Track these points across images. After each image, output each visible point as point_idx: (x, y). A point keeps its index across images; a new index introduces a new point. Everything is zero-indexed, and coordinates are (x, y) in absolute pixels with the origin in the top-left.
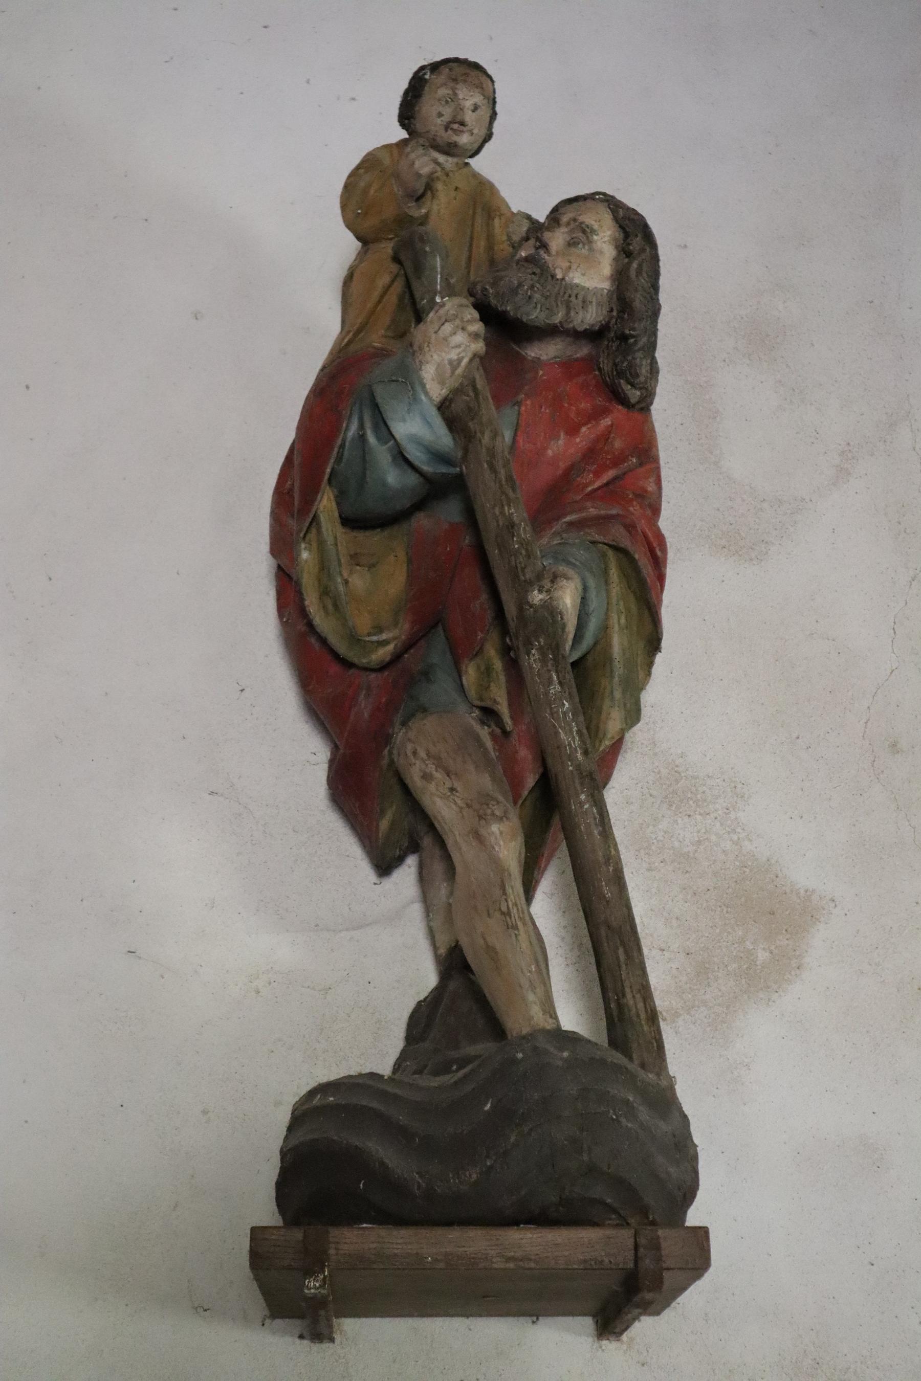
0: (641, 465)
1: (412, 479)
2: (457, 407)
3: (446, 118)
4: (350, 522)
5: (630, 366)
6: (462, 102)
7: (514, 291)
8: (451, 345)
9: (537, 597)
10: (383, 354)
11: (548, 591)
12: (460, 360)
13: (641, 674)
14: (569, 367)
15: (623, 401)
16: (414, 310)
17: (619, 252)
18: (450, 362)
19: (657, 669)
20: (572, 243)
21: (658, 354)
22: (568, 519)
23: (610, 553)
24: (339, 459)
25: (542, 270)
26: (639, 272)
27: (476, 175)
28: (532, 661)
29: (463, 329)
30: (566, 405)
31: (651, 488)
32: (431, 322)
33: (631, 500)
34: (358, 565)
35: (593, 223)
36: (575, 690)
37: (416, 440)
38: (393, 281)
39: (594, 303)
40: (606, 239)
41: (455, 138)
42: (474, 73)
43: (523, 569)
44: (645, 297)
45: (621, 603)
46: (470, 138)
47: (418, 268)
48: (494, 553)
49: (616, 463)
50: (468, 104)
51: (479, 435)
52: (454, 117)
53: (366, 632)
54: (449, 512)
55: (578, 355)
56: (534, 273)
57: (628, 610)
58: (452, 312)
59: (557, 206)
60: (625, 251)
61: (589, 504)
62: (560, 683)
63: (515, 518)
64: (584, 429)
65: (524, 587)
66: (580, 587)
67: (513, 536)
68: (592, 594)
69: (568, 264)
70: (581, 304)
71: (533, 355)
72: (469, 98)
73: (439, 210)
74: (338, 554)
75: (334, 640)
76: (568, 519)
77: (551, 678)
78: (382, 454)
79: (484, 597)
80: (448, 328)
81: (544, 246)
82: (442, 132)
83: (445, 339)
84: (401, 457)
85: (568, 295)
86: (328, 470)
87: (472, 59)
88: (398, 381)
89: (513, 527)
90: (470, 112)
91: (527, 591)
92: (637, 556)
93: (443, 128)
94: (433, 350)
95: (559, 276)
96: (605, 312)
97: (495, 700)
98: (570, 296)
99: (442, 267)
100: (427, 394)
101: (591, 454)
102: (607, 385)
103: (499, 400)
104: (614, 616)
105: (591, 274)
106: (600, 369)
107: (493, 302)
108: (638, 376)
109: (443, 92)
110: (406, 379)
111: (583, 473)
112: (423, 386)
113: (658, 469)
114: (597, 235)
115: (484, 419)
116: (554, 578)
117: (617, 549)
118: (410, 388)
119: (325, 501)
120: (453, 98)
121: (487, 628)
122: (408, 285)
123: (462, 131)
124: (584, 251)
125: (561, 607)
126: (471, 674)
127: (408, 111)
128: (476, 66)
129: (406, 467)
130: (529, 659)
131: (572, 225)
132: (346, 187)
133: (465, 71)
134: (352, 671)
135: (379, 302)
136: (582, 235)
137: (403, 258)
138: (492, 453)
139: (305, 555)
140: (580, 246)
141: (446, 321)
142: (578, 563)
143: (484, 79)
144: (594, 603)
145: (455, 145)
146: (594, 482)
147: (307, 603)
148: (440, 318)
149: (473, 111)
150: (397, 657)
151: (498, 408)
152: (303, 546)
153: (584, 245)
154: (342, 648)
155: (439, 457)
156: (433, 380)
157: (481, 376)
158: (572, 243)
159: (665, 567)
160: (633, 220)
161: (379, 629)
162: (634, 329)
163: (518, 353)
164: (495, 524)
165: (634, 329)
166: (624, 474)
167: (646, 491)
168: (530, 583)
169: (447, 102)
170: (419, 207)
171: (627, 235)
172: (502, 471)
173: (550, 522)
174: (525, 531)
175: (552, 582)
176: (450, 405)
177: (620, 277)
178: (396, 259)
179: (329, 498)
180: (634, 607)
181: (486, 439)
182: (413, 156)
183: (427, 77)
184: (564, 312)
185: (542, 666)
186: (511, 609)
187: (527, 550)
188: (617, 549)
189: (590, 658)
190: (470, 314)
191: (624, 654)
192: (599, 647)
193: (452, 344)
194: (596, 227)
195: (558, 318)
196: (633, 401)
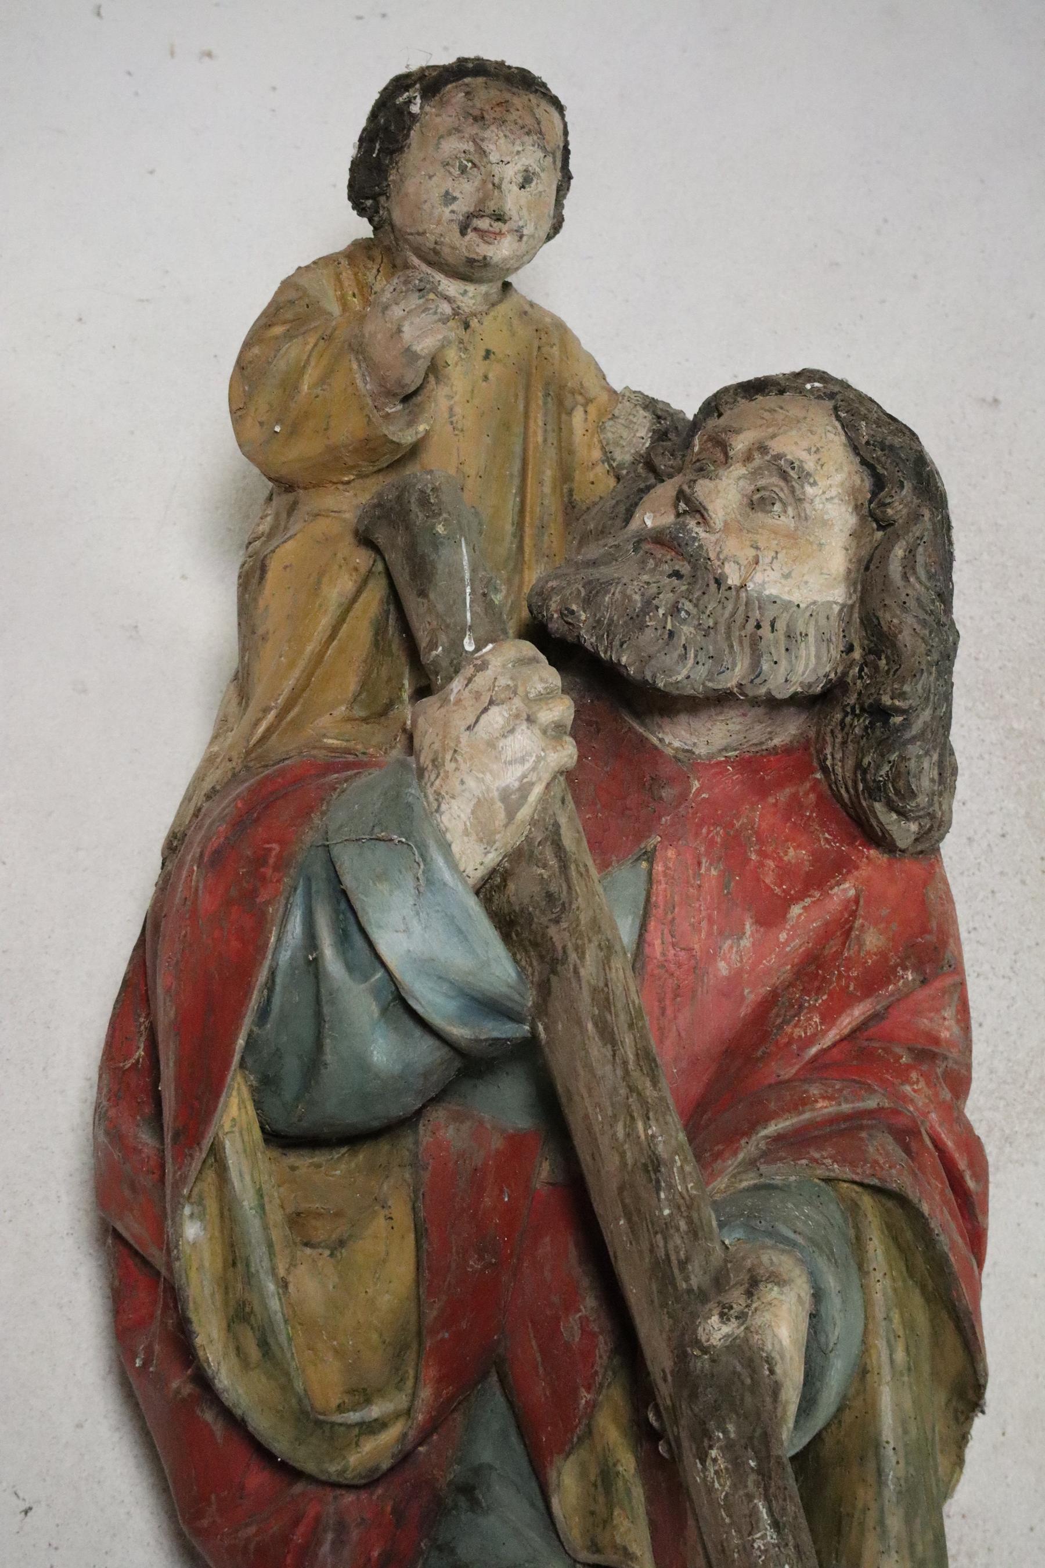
0: (924, 982)
1: (424, 1052)
2: (522, 890)
3: (462, 206)
4: (279, 1138)
5: (898, 774)
6: (496, 170)
7: (637, 621)
8: (504, 749)
9: (716, 1331)
10: (348, 764)
11: (742, 1317)
12: (524, 789)
13: (943, 1462)
14: (754, 767)
15: (882, 841)
16: (413, 662)
17: (862, 519)
18: (505, 795)
19: (972, 1452)
20: (758, 502)
21: (957, 737)
22: (772, 1128)
23: (867, 1201)
24: (263, 1014)
25: (695, 567)
26: (909, 563)
27: (528, 312)
28: (712, 1473)
29: (530, 720)
30: (754, 857)
31: (948, 1030)
32: (458, 701)
33: (909, 1067)
34: (306, 1244)
35: (804, 455)
36: (806, 1537)
37: (427, 966)
38: (359, 592)
39: (811, 639)
40: (833, 492)
41: (484, 250)
42: (520, 100)
43: (683, 1265)
44: (924, 623)
45: (896, 1317)
46: (516, 245)
47: (422, 571)
48: (616, 1227)
49: (870, 986)
50: (511, 172)
51: (573, 956)
52: (482, 201)
53: (335, 1402)
54: (505, 1104)
55: (777, 741)
56: (677, 575)
57: (909, 1325)
58: (503, 681)
59: (716, 396)
60: (874, 515)
61: (815, 1090)
62: (776, 1525)
63: (660, 1148)
64: (796, 910)
65: (685, 1308)
66: (807, 1298)
67: (658, 1189)
68: (834, 1305)
69: (752, 552)
70: (783, 643)
71: (677, 744)
72: (512, 156)
73: (451, 409)
74: (266, 1228)
75: (261, 1423)
76: (772, 1128)
77: (754, 1513)
78: (358, 1003)
79: (589, 1303)
80: (497, 717)
81: (698, 511)
82: (453, 237)
83: (491, 744)
84: (399, 1005)
85: (755, 625)
86: (241, 1042)
87: (514, 61)
88: (391, 840)
89: (657, 1170)
90: (515, 188)
91: (694, 1316)
92: (925, 1208)
93: (456, 228)
94: (464, 767)
95: (733, 579)
96: (835, 654)
97: (625, 1549)
98: (758, 626)
99: (474, 570)
100: (453, 865)
101: (812, 970)
102: (844, 805)
103: (604, 848)
104: (880, 1344)
105: (799, 571)
106: (825, 770)
107: (589, 640)
108: (913, 795)
109: (452, 146)
110: (404, 829)
111: (798, 1014)
112: (446, 847)
113: (963, 984)
114: (814, 484)
115: (584, 918)
116: (753, 1285)
117: (879, 1191)
118: (418, 858)
119: (234, 1110)
120: (474, 162)
121: (598, 1379)
122: (394, 597)
123: (500, 233)
124: (787, 521)
125: (769, 1347)
126: (568, 1484)
127: (371, 179)
128: (525, 81)
129: (409, 1024)
130: (705, 1468)
131: (758, 460)
132: (241, 366)
133: (500, 90)
134: (299, 1488)
135: (332, 637)
136: (779, 484)
137: (381, 538)
138: (603, 998)
139: (191, 1230)
140: (777, 507)
141: (491, 702)
142: (800, 1240)
143: (544, 109)
144: (842, 1328)
145: (485, 263)
146: (824, 1033)
147: (199, 1341)
148: (478, 695)
149: (523, 187)
150: (404, 1458)
151: (604, 866)
152: (187, 1211)
153: (785, 505)
154: (282, 1445)
155: (487, 1005)
156: (466, 833)
157: (570, 819)
158: (758, 502)
159: (985, 1212)
160: (891, 447)
161: (364, 1396)
162: (902, 695)
163: (643, 740)
164: (617, 1159)
165: (902, 695)
166: (887, 1008)
167: (936, 1041)
168: (703, 1297)
169: (463, 170)
170: (411, 423)
171: (879, 483)
172: (628, 1040)
173: (732, 1138)
174: (682, 1173)
175: (749, 1294)
176: (504, 880)
177: (868, 574)
178: (365, 540)
179: (242, 1102)
180: (922, 1319)
181: (589, 969)
182: (397, 312)
183: (415, 109)
184: (747, 661)
185: (734, 1486)
186: (658, 1354)
187: (690, 1221)
188: (879, 1191)
189: (829, 1441)
190: (542, 680)
191: (906, 1432)
192: (848, 1417)
193: (508, 755)
194: (810, 465)
195: (730, 681)
196: (901, 844)
